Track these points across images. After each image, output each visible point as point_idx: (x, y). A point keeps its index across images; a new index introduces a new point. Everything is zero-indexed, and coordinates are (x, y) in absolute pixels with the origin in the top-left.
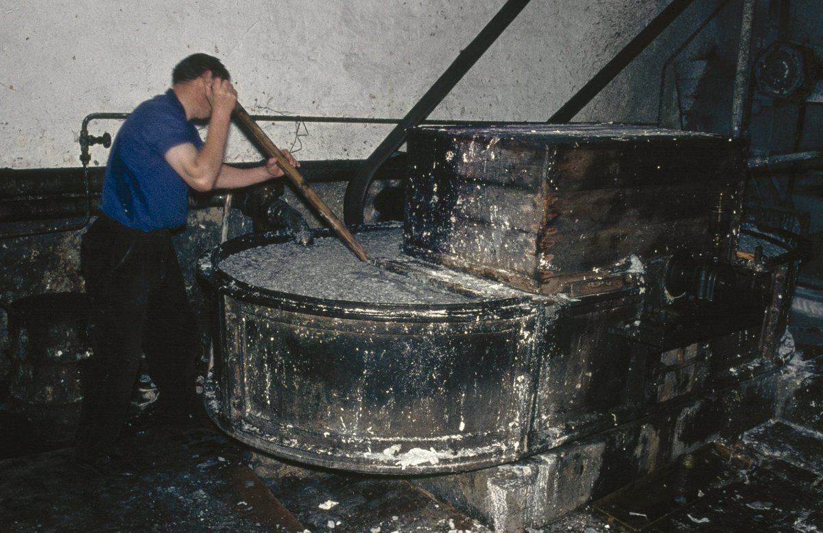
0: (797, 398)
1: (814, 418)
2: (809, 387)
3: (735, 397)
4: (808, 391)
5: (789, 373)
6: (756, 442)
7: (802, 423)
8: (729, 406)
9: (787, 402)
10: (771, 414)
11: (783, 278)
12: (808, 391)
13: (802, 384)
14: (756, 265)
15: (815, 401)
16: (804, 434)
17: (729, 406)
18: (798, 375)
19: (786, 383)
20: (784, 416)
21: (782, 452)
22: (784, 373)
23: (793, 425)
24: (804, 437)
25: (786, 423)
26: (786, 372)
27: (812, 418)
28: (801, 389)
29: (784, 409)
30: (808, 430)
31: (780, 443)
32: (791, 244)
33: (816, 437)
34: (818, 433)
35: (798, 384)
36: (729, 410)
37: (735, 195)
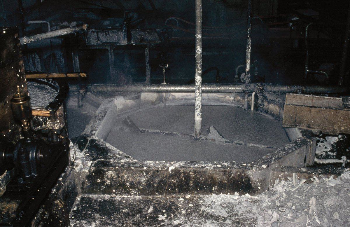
0: (89, 180)
1: (102, 188)
2: (94, 172)
3: (59, 205)
4: (94, 174)
5: (78, 166)
6: (78, 222)
7: (95, 193)
8: (58, 214)
9: (83, 184)
10: (76, 195)
11: (62, 114)
12: (94, 174)
13: (89, 171)
14: (54, 125)
15: (100, 179)
16: (99, 200)
17: (58, 214)
18: (84, 165)
19: (79, 173)
20: (84, 192)
21: (95, 222)
22: (76, 167)
23: (90, 196)
24: (100, 202)
25: (86, 196)
26: (77, 166)
27: (100, 189)
28: (90, 174)
29: (82, 188)
30: (100, 196)
31: (90, 214)
32: (52, 82)
33: (106, 199)
34: (106, 195)
35: (87, 172)
36: (58, 216)
37: (19, 73)
